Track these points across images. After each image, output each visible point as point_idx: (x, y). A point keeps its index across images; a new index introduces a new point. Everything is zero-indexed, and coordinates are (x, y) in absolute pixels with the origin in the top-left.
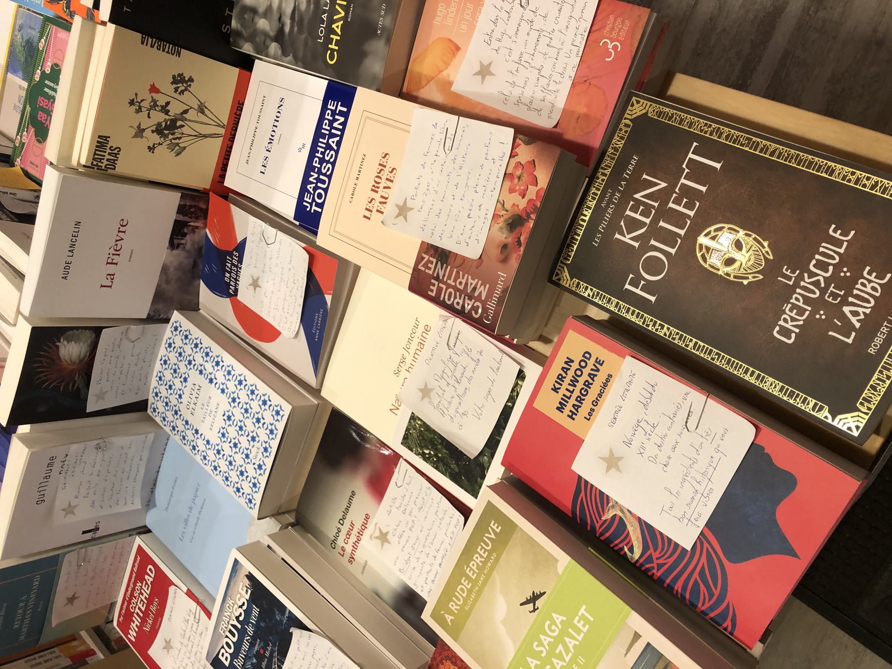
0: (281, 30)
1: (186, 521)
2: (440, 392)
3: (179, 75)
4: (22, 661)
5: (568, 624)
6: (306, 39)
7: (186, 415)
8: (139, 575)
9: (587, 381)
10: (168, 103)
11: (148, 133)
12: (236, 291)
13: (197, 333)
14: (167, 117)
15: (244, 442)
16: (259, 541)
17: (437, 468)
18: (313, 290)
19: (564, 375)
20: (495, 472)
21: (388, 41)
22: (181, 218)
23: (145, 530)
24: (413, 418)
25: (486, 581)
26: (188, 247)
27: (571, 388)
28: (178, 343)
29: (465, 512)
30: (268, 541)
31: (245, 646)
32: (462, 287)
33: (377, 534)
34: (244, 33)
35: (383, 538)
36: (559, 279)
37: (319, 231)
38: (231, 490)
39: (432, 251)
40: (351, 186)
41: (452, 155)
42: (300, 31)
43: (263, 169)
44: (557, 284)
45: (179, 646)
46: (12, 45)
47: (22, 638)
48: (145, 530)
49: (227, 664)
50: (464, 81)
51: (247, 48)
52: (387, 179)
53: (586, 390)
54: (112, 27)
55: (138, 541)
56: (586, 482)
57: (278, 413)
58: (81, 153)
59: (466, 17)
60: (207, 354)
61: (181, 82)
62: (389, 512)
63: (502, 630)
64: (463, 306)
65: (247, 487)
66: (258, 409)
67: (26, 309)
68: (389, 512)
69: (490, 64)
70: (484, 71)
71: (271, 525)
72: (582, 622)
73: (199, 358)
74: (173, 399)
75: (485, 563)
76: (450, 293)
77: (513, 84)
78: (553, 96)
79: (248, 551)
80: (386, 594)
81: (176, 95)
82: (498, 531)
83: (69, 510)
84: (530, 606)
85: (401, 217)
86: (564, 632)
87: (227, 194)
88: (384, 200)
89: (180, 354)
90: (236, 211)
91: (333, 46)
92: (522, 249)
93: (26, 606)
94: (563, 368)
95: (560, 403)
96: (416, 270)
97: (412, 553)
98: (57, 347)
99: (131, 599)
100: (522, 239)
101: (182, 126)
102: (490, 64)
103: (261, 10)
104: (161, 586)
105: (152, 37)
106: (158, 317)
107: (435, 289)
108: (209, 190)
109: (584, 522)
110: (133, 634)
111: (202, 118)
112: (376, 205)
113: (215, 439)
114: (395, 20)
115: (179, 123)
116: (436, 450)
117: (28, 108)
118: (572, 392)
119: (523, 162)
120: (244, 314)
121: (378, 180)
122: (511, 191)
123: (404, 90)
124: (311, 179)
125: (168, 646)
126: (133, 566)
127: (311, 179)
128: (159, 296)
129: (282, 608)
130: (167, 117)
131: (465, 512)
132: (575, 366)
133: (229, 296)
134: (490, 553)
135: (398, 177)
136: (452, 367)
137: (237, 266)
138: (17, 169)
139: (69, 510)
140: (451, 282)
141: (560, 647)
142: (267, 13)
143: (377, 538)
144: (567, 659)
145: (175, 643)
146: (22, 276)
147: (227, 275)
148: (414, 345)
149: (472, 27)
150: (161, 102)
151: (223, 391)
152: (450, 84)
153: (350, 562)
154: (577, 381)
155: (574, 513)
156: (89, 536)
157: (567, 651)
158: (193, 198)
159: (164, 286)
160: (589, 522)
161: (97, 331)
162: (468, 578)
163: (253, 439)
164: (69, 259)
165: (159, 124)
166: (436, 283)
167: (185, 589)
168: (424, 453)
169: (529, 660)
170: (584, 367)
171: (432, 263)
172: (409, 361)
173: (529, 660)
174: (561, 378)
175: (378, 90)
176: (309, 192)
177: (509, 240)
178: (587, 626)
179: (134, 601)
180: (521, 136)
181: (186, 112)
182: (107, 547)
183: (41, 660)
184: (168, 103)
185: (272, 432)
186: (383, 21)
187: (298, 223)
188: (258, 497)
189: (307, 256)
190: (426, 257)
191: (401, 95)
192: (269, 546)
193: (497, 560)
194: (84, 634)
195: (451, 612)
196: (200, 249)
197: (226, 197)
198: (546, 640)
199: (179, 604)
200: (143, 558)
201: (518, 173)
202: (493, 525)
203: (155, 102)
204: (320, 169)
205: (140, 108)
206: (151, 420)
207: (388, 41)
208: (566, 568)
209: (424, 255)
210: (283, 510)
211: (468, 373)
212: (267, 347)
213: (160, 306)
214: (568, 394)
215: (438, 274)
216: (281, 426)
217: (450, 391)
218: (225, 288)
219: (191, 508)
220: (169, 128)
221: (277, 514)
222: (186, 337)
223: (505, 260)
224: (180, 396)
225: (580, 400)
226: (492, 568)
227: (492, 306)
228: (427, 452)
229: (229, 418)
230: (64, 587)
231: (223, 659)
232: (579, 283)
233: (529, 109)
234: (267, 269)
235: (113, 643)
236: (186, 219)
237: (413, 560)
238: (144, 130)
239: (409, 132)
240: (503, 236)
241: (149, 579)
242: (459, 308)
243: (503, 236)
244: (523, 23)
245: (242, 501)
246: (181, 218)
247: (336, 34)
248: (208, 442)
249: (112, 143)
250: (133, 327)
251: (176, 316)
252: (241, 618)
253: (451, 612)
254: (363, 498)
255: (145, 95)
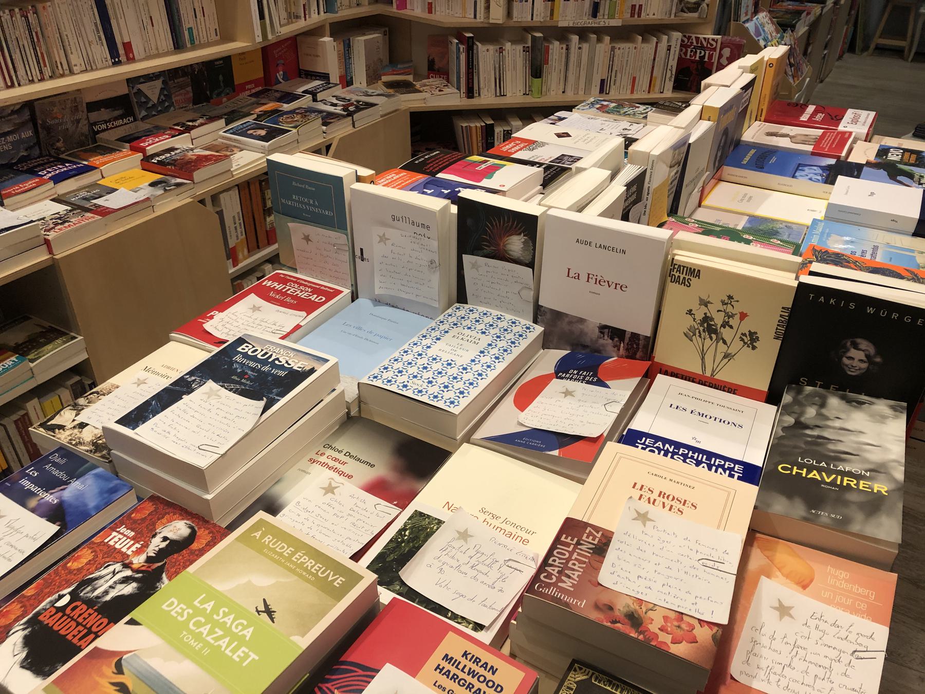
0: (807, 427)
1: (360, 328)
2: (463, 549)
3: (757, 338)
4: (239, 210)
5: (241, 641)
6: (800, 448)
7: (451, 333)
8: (317, 291)
9: (473, 686)
10: (731, 327)
11: (704, 309)
12: (562, 378)
13: (524, 344)
14: (719, 326)
15: (427, 375)
16: (339, 382)
17: (391, 541)
18: (564, 440)
19: (480, 664)
20: (386, 596)
21: (806, 519)
22: (627, 336)
23: (354, 297)
24: (440, 522)
25: (290, 570)
26: (601, 341)
27: (466, 670)
28: (515, 329)
29: (356, 557)
30: (339, 389)
31: (252, 364)
32: (570, 565)
33: (334, 485)
34: (801, 397)
35: (330, 490)
36: (575, 670)
37: (621, 445)
38: (386, 363)
39: (604, 541)
40: (664, 474)
41: (697, 564)
42: (807, 443)
43: (674, 406)
44: (570, 668)
45: (254, 317)
46: (773, 220)
47: (283, 201)
48: (354, 297)
49: (239, 349)
50: (771, 590)
51: (787, 398)
52: (672, 506)
53: (464, 685)
54: (795, 284)
55: (346, 291)
56: (373, 677)
57: (452, 403)
58: (684, 257)
59: (838, 598)
60: (505, 351)
61: (752, 339)
62: (352, 496)
63: (243, 580)
64: (551, 565)
65: (388, 375)
66: (456, 387)
67: (552, 212)
68: (352, 496)
69: (791, 616)
70: (783, 610)
71: (352, 393)
72: (242, 655)
73: (502, 344)
74: (468, 323)
75: (306, 569)
76: (564, 555)
77: (773, 638)
78: (764, 678)
79: (334, 372)
80: (277, 489)
81: (739, 335)
82: (335, 584)
83: (383, 239)
84: (262, 608)
85: (636, 515)
86: (234, 637)
87: (649, 376)
88: (652, 501)
89: (506, 330)
90: (635, 381)
91: (795, 470)
92: (609, 624)
93: (309, 205)
94: (486, 664)
95: (452, 658)
96: (586, 525)
97: (313, 514)
98: (520, 234)
99: (298, 283)
100: (618, 625)
101: (711, 338)
102: (791, 616)
103: (824, 411)
104: (307, 306)
105: (790, 316)
106: (539, 313)
107: (568, 540)
108: (653, 361)
109: (334, 672)
110: (269, 284)
111: (720, 356)
112: (647, 495)
113: (430, 352)
114: (826, 526)
115: (714, 336)
116: (408, 541)
117: (719, 229)
118: (462, 670)
119: (694, 631)
120: (540, 384)
121: (671, 498)
122: (666, 618)
123: (758, 535)
124: (667, 446)
125: (255, 309)
126: (325, 287)
127: (667, 446)
128: (558, 315)
129: (283, 395)
130: (719, 326)
131: (356, 557)
132: (489, 676)
133: (557, 372)
134: (315, 575)
135: (673, 516)
136: (487, 562)
137: (583, 379)
138: (666, 218)
139: (383, 239)
140: (575, 556)
141: (220, 633)
142: (820, 415)
143: (330, 484)
144: (209, 639)
145: (257, 314)
146: (580, 210)
147: (575, 372)
148: (509, 528)
149: (828, 602)
150: (732, 322)
151: (473, 361)
152: (768, 577)
153: (311, 460)
154: (473, 677)
155: (343, 663)
156: (358, 253)
157: (217, 639)
158: (645, 346)
159: (567, 320)
160: (334, 677)
161: (531, 265)
162: (294, 554)
163: (430, 382)
164: (593, 245)
165: (712, 319)
166: (574, 542)
167: (302, 324)
168: (406, 530)
169: (212, 603)
170: (487, 685)
171: (593, 540)
172: (495, 522)
173: (212, 603)
174: (477, 661)
175: (755, 507)
176: (655, 443)
177: (617, 613)
178: (238, 660)
179: (296, 286)
180: (720, 632)
181: (725, 342)
182: (346, 268)
183: (237, 225)
184: (731, 327)
185: (436, 397)
186: (825, 516)
187: (625, 433)
188: (379, 383)
189: (595, 436)
190: (599, 535)
191: (752, 534)
192: (334, 390)
193: (308, 581)
194: (276, 246)
195: (262, 536)
196: (599, 351)
197: (646, 375)
198: (229, 620)
199: (290, 318)
200: (331, 294)
201: (684, 626)
202: (340, 580)
203: (732, 316)
204: (677, 453)
205: (726, 304)
206: (449, 306)
207: (806, 519)
208: (295, 644)
209: (600, 533)
210: (362, 405)
211: (481, 577)
212: (510, 400)
213: (548, 316)
214: (461, 667)
215: (582, 544)
216: (440, 404)
217: (464, 559)
218: (563, 369)
219: (371, 332)
220: (708, 327)
221: (360, 400)
222: (521, 336)
223: (597, 607)
224: (469, 328)
225: (454, 678)
226: (300, 576)
227: (552, 591)
228: (407, 533)
229: (449, 364)
230: (318, 233)
231: (243, 347)
232: (572, 689)
233: (749, 652)
234: (581, 403)
235: (239, 281)
236: (627, 340)
237: (306, 515)
238: (706, 306)
239: (718, 527)
240: (621, 607)
241: (313, 298)
242: (550, 562)
243: (621, 607)
244: (836, 653)
245: (376, 371)
246: (627, 336)
247: (807, 474)
248: (429, 347)
249: (694, 281)
250: (532, 293)
251: (539, 329)
252: (277, 362)
253: (262, 536)
254: (368, 474)
255: (737, 309)
